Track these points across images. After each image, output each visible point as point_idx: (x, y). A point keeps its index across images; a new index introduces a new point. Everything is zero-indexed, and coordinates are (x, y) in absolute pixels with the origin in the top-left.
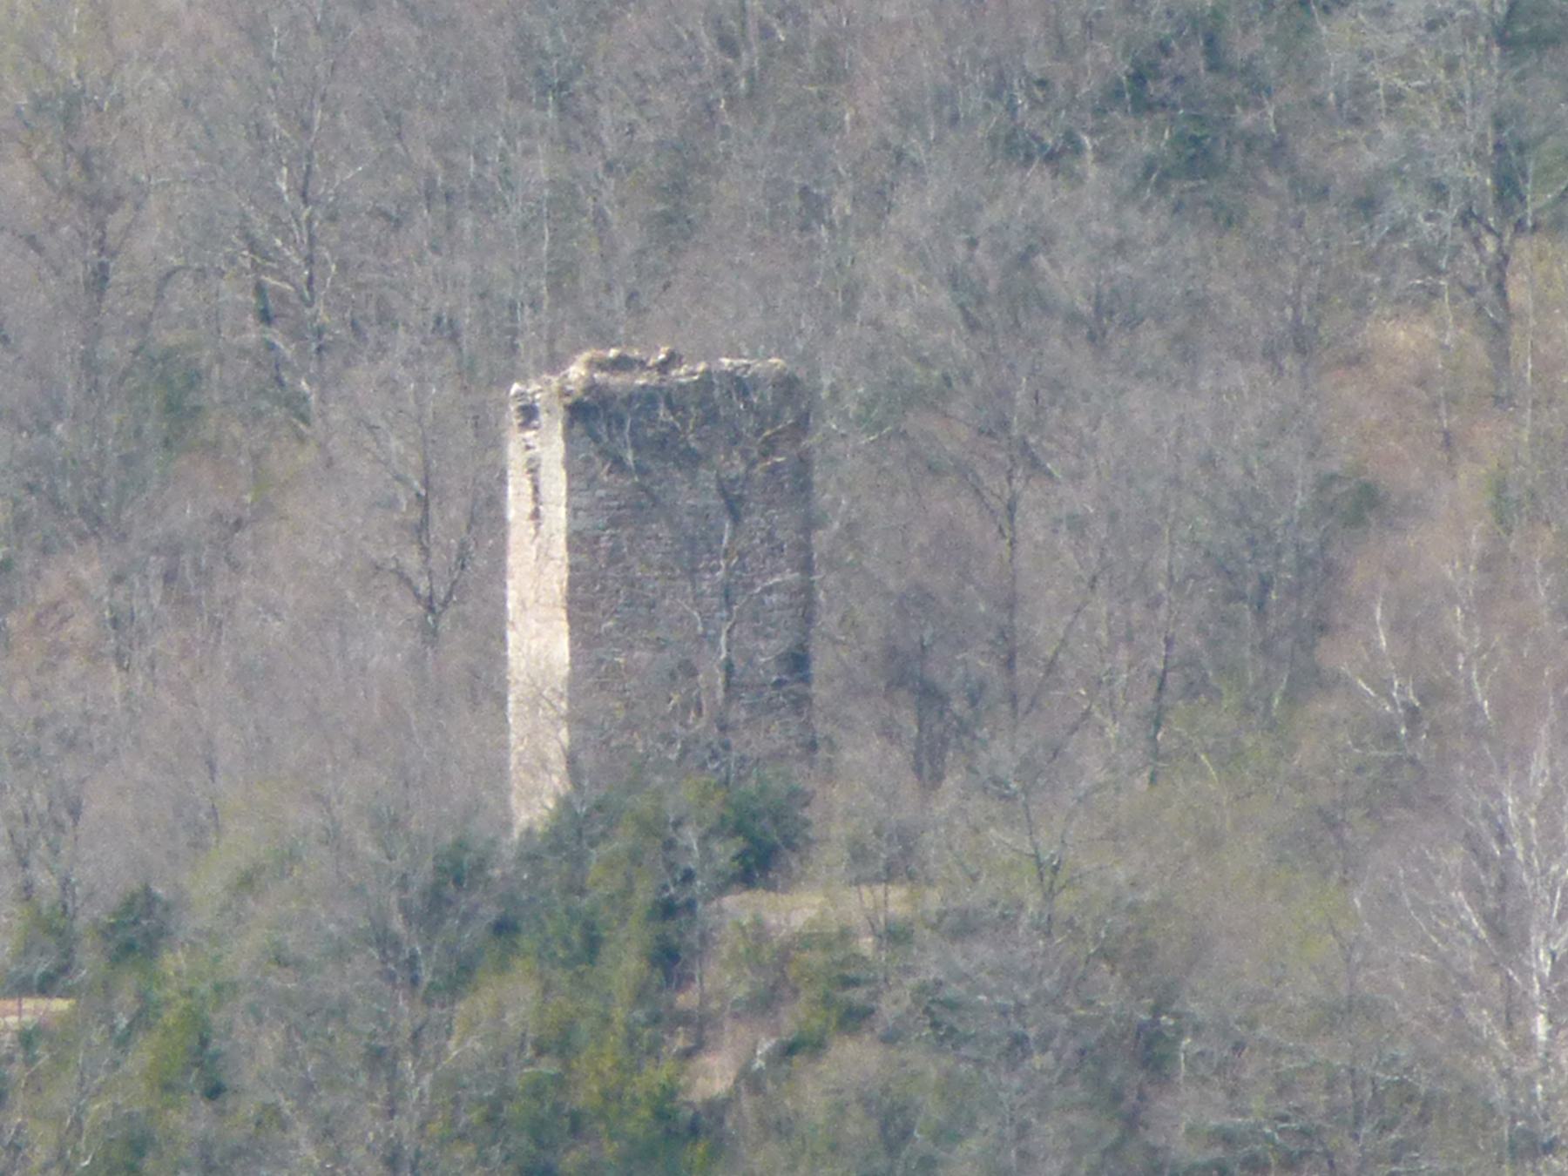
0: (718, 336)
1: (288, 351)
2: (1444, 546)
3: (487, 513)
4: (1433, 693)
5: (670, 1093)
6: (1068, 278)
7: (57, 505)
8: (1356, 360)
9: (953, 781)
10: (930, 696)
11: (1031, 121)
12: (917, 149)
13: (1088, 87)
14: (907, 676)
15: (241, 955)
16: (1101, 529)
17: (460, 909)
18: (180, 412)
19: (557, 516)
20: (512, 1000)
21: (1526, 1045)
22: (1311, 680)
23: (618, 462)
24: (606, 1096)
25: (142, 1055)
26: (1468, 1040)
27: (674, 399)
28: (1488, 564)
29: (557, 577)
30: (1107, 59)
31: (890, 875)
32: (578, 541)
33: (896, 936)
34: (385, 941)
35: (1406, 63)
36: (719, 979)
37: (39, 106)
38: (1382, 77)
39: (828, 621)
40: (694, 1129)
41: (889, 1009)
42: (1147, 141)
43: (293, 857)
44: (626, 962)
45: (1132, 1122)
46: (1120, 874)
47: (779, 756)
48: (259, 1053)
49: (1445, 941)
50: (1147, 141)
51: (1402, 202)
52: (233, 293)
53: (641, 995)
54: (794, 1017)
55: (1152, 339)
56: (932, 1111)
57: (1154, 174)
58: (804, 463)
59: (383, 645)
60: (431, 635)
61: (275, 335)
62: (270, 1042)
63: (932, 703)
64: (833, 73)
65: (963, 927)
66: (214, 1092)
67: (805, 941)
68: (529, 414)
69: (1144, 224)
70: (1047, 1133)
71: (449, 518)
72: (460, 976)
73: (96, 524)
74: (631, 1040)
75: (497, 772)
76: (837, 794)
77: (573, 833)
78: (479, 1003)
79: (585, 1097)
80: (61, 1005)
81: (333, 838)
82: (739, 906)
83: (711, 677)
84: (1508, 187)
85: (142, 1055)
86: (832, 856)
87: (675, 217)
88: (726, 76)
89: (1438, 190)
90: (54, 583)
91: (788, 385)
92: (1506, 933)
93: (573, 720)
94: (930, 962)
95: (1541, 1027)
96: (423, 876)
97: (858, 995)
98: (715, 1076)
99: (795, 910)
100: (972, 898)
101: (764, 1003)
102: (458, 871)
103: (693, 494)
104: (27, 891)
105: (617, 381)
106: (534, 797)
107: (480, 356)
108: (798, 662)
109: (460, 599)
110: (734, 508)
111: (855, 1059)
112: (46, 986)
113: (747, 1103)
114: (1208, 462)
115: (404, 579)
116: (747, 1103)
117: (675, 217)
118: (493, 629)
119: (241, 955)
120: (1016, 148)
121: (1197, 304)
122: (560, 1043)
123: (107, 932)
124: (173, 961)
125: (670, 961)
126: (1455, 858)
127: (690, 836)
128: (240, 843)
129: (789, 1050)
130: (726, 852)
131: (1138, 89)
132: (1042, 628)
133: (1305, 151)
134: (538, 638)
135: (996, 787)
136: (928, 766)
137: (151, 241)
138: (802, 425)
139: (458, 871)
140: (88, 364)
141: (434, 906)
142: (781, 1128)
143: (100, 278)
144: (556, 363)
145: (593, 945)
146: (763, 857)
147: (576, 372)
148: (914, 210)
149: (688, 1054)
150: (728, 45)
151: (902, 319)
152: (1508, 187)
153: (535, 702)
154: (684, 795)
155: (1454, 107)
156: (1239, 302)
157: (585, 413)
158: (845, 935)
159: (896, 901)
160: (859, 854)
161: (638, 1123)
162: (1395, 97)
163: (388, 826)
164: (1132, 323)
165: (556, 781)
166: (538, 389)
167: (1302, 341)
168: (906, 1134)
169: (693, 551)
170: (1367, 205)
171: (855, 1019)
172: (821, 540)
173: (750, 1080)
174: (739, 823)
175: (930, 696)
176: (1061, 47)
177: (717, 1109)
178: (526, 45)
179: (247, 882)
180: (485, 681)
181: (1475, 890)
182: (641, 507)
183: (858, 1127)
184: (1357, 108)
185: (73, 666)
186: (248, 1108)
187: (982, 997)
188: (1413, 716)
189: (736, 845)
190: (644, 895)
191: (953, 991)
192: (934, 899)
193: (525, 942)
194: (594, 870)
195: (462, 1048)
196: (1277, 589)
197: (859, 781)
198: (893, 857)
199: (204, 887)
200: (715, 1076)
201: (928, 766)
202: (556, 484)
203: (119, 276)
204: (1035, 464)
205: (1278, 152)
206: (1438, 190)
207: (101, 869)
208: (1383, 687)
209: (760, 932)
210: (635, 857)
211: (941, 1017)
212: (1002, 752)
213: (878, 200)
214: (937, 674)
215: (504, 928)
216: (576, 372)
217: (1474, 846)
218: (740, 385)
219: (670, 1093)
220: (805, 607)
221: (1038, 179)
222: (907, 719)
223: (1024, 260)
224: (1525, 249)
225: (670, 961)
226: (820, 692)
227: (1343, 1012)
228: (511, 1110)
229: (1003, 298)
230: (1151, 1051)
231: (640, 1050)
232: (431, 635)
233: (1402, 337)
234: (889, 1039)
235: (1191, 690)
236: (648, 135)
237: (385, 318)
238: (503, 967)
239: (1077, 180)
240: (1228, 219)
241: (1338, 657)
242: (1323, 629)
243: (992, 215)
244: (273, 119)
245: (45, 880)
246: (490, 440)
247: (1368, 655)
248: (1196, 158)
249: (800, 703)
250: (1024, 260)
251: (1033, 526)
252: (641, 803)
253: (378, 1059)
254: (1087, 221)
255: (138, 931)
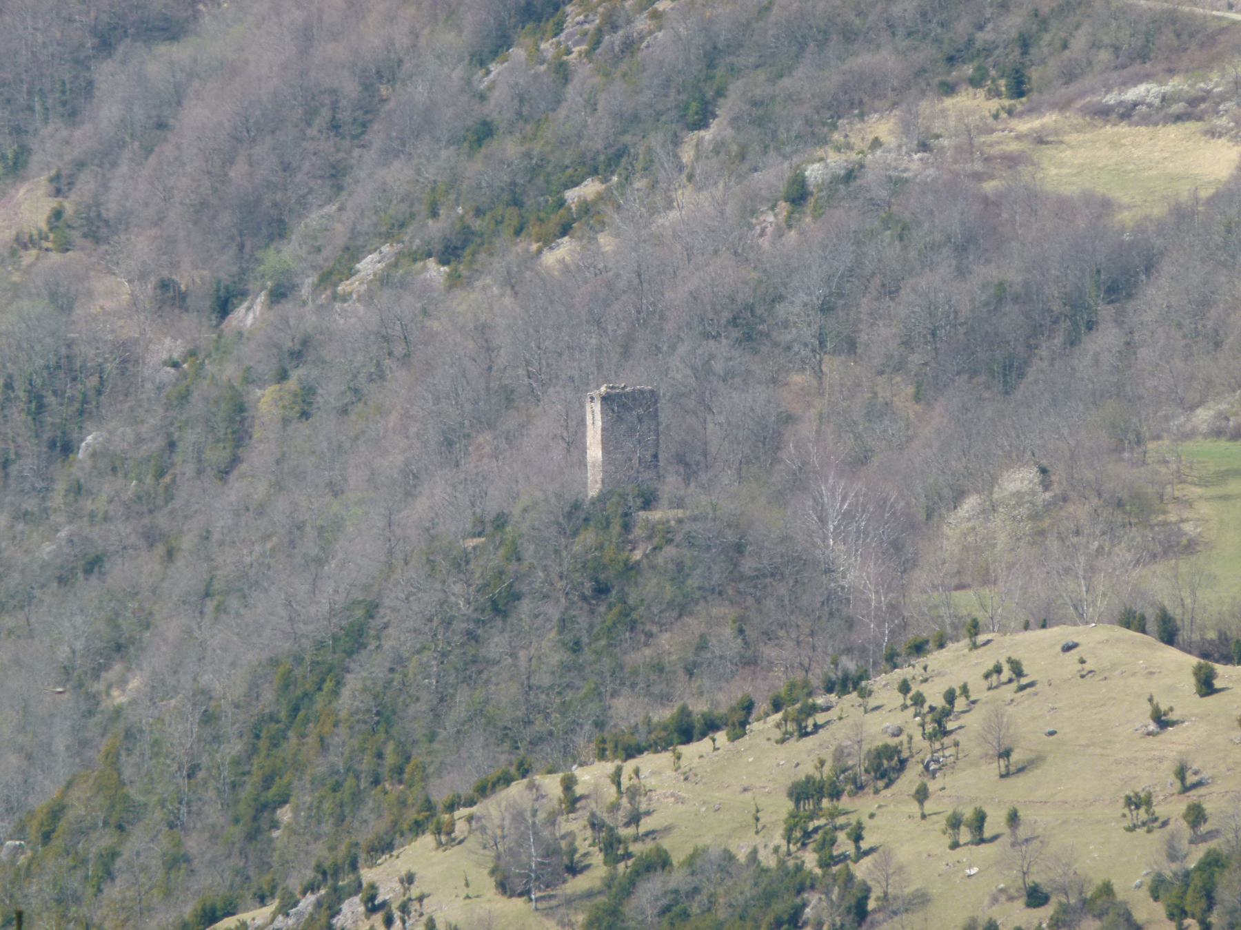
0: (634, 380)
1: (535, 385)
2: (807, 429)
3: (582, 422)
4: (804, 463)
5: (627, 560)
6: (718, 366)
7: (481, 422)
8: (787, 384)
9: (692, 485)
10: (687, 465)
11: (709, 329)
12: (682, 335)
13: (723, 321)
14: (681, 460)
15: (524, 527)
16: (725, 426)
17: (576, 515)
18: (509, 400)
19: (599, 424)
20: (589, 537)
21: (828, 545)
22: (776, 460)
23: (613, 411)
24: (611, 560)
25: (502, 551)
26: (814, 545)
27: (626, 395)
28: (818, 432)
29: (599, 437)
30: (726, 315)
31: (678, 507)
32: (603, 429)
33: (680, 521)
34: (559, 524)
35: (798, 315)
36: (638, 532)
37: (476, 328)
38: (792, 319)
39: (663, 446)
40: (632, 568)
41: (679, 538)
42: (736, 334)
43: (537, 503)
44: (616, 528)
45: (736, 565)
46: (732, 506)
47: (651, 479)
48: (529, 550)
49: (687, 107)
50: (736, 334)
51: (796, 348)
52: (521, 372)
53: (620, 535)
54: (655, 541)
55: (738, 380)
56: (688, 563)
57: (739, 341)
58: (656, 410)
59: (557, 452)
60: (569, 451)
61: (531, 381)
62: (532, 547)
63: (688, 466)
64: (662, 317)
65: (695, 519)
66: (519, 560)
67: (659, 523)
68: (592, 398)
69: (736, 353)
70: (715, 568)
71: (572, 424)
72: (575, 533)
73: (491, 426)
74: (617, 546)
75: (585, 485)
76: (666, 489)
77: (602, 498)
78: (579, 539)
79: (606, 560)
80: (483, 539)
81: (546, 500)
82: (642, 514)
83: (635, 461)
84: (822, 344)
85: (502, 551)
86: (664, 502)
87: (626, 353)
88: (638, 319)
89: (806, 345)
90: (481, 439)
91: (652, 392)
92: (822, 520)
93: (605, 472)
94: (687, 527)
95: (831, 542)
96: (567, 509)
97: (670, 536)
98: (637, 555)
99: (656, 515)
100: (696, 512)
101: (650, 538)
102: (576, 506)
103: (631, 417)
104: (474, 513)
105: (614, 391)
106: (593, 491)
107: (580, 386)
108: (655, 456)
109: (576, 443)
110: (640, 420)
111: (670, 551)
112: (480, 535)
113: (645, 561)
114: (752, 410)
115: (563, 438)
116: (645, 561)
117: (626, 353)
118: (584, 451)
119: (524, 527)
120: (706, 336)
121: (748, 371)
122: (601, 547)
123: (492, 522)
124: (508, 529)
125: (626, 527)
126: (810, 503)
127: (630, 498)
128: (525, 500)
129: (655, 549)
130: (639, 502)
131: (734, 321)
132: (713, 449)
133: (774, 334)
134: (595, 452)
135: (702, 486)
136: (687, 480)
137: (502, 359)
138: (656, 402)
139: (576, 506)
140: (488, 389)
141: (569, 515)
142: (653, 567)
143: (490, 368)
144: (598, 387)
145: (608, 524)
146: (648, 502)
147: (603, 389)
148: (682, 349)
149: (631, 551)
150: (639, 312)
151: (679, 377)
152: (822, 344)
153: (594, 466)
154: (629, 489)
155: (809, 325)
156: (758, 371)
157: (605, 399)
158: (668, 521)
159: (680, 513)
160: (671, 502)
161: (620, 567)
162: (795, 323)
163: (559, 496)
164: (733, 378)
165: (599, 485)
166: (595, 393)
167: (774, 381)
168: (683, 569)
169: (631, 431)
170: (788, 348)
171: (669, 541)
172: (661, 428)
173: (646, 556)
174: (641, 495)
175: (687, 465)
176: (716, 312)
177: (638, 563)
178: (590, 311)
179: (525, 510)
180: (582, 463)
181: (815, 510)
182: (620, 419)
183: (671, 566)
184: (786, 325)
185: (485, 460)
186: (526, 564)
187: (751, 759)
188: (800, 468)
189: (642, 500)
190: (620, 511)
191: (693, 534)
192: (688, 513)
193: (592, 523)
194: (608, 505)
195: (577, 548)
196: (768, 438)
197: (671, 484)
198: (680, 503)
199: (516, 511)
200: (637, 555)
201: (687, 480)
202: (598, 416)
203: (495, 368)
204: (710, 409)
205: (768, 335)
206: (806, 345)
207: (492, 507)
208: (792, 461)
209: (647, 520)
210: (618, 503)
211: (690, 541)
212: (704, 477)
213: (673, 348)
214: (688, 460)
215: (586, 520)
216: (603, 389)
217: (815, 500)
218: (642, 392)
219: (627, 560)
220: (657, 444)
221: (712, 342)
222: (682, 470)
223: (708, 362)
224: (826, 358)
225: (626, 527)
226: (661, 464)
227: (784, 539)
228: (589, 564)
229: (703, 371)
230: (739, 548)
231: (620, 548)
232: (569, 451)
233: (797, 379)
234: (677, 546)
235: (747, 463)
236: (619, 332)
237: (557, 377)
238: (586, 529)
239: (720, 343)
240: (756, 352)
241: (782, 455)
242: (778, 448)
243: (699, 352)
244: (531, 331)
245: (478, 510)
246: (582, 407)
247: (789, 453)
248: (749, 337)
249: (656, 466)
250: (708, 362)
251: (710, 426)
252: (619, 490)
253: (557, 552)
254: (723, 352)
255: (500, 522)
